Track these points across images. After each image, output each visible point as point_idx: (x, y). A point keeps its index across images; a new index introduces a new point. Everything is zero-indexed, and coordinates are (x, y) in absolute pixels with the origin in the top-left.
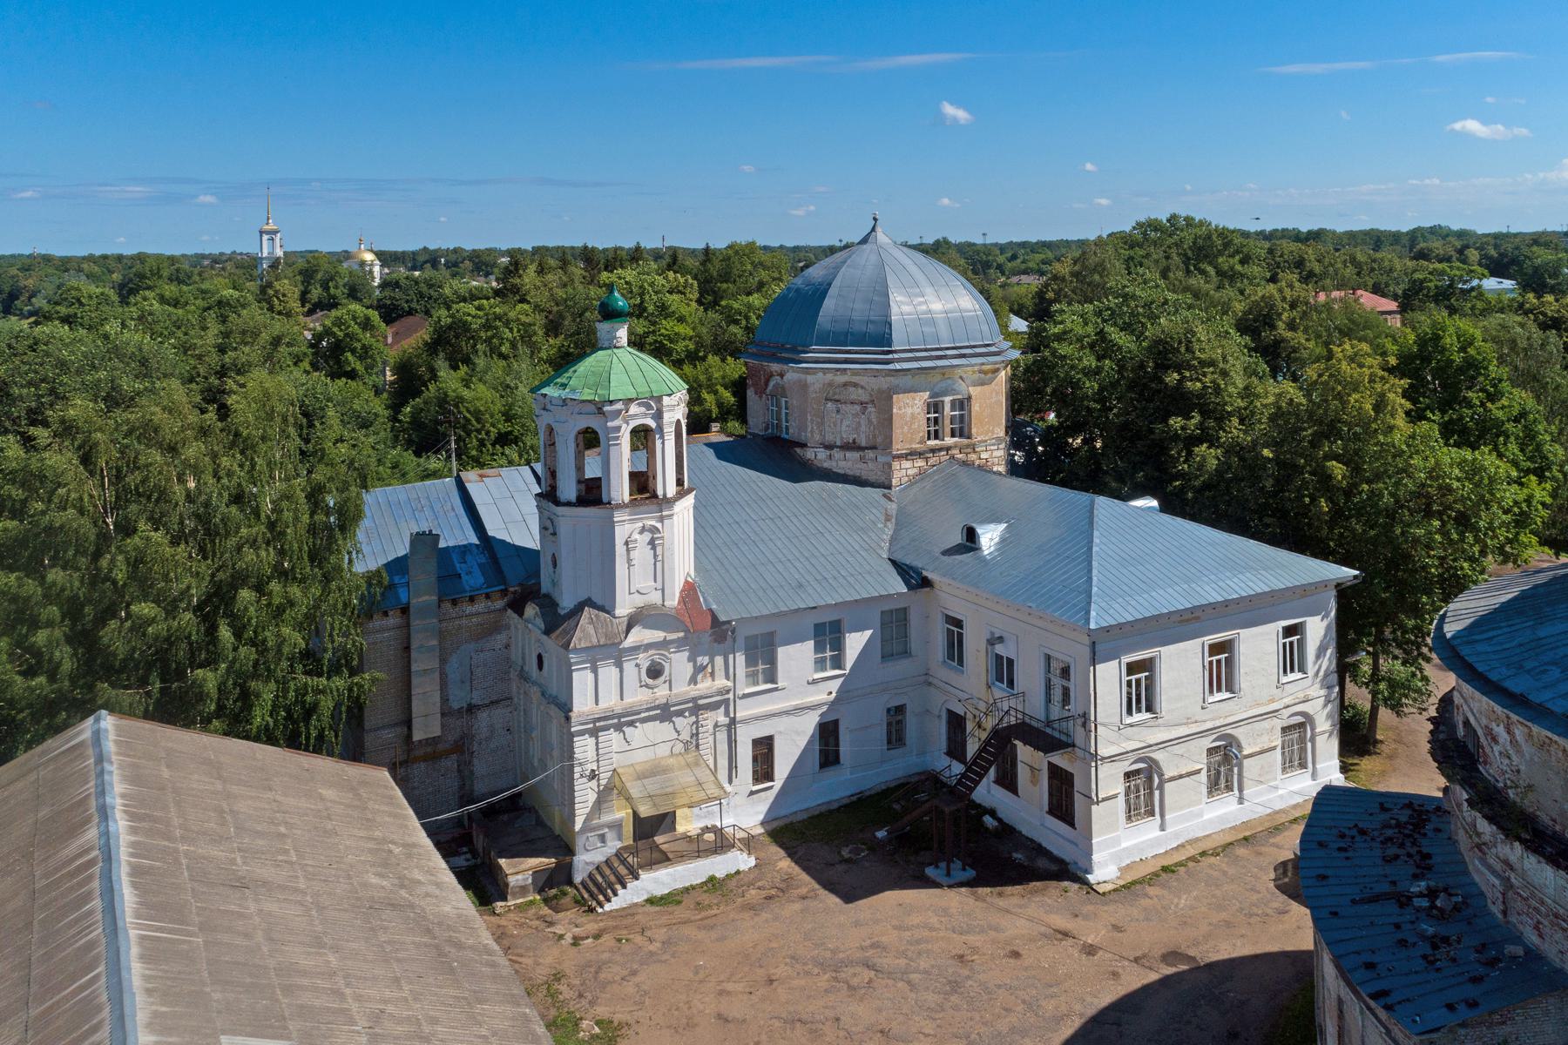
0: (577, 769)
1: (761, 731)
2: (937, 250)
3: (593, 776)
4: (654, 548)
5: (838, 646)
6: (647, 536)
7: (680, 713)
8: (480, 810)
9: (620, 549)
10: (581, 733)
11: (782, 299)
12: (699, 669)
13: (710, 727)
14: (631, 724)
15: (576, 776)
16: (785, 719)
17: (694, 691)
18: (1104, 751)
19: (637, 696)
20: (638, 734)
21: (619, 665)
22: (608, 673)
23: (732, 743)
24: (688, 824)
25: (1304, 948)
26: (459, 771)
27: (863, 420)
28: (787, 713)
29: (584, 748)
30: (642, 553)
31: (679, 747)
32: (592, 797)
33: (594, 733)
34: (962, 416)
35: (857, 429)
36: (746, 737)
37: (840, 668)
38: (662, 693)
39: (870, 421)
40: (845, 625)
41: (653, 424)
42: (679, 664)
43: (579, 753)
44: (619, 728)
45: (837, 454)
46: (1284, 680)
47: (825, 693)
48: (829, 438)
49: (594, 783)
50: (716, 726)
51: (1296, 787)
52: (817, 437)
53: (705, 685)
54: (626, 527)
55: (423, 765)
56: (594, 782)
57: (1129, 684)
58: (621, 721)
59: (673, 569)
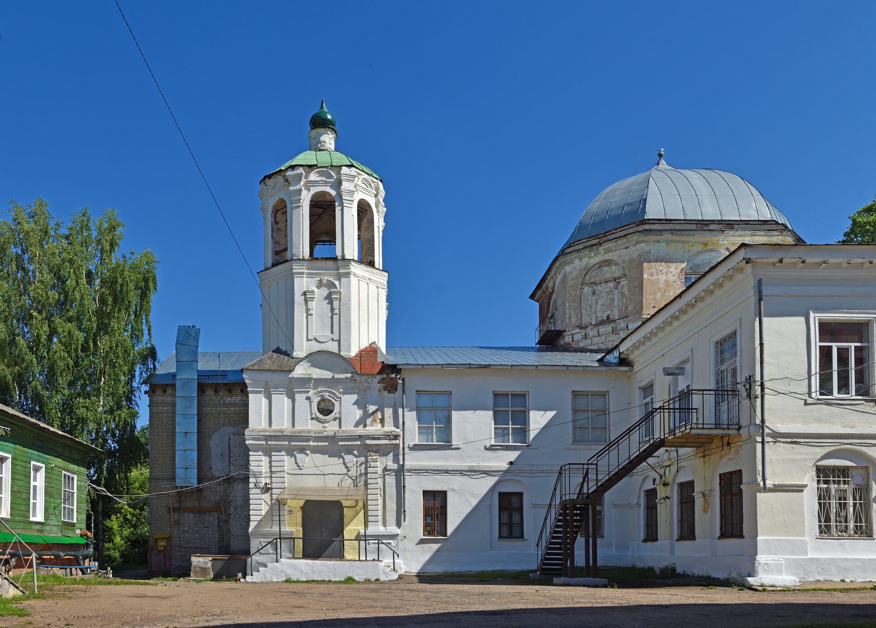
0: (251, 480)
1: (435, 484)
2: (459, 449)
3: (267, 489)
4: (331, 303)
5: (522, 419)
6: (325, 291)
7: (349, 451)
8: (7, 405)
9: (298, 299)
10: (257, 449)
11: (653, 444)
12: (366, 415)
13: (380, 471)
14: (302, 450)
15: (251, 485)
16: (459, 478)
17: (360, 430)
18: (774, 423)
19: (307, 424)
20: (307, 460)
21: (292, 396)
22: (282, 402)
23: (400, 489)
24: (568, 339)
25: (171, 371)
26: (219, 527)
27: (616, 295)
28: (461, 472)
29: (258, 463)
30: (318, 305)
31: (348, 482)
32: (265, 509)
33: (268, 452)
34: (723, 361)
35: (610, 306)
36: (415, 489)
37: (399, 436)
38: (332, 428)
39: (622, 294)
40: (531, 400)
41: (333, 193)
42: (348, 407)
43: (253, 467)
44: (290, 452)
45: (592, 332)
46: (653, 377)
47: (501, 461)
48: (585, 320)
49: (266, 497)
50: (385, 469)
51: (201, 559)
52: (574, 320)
53: (374, 428)
54: (304, 283)
55: (192, 515)
56: (268, 495)
57: (825, 353)
58: (293, 444)
59: (349, 323)
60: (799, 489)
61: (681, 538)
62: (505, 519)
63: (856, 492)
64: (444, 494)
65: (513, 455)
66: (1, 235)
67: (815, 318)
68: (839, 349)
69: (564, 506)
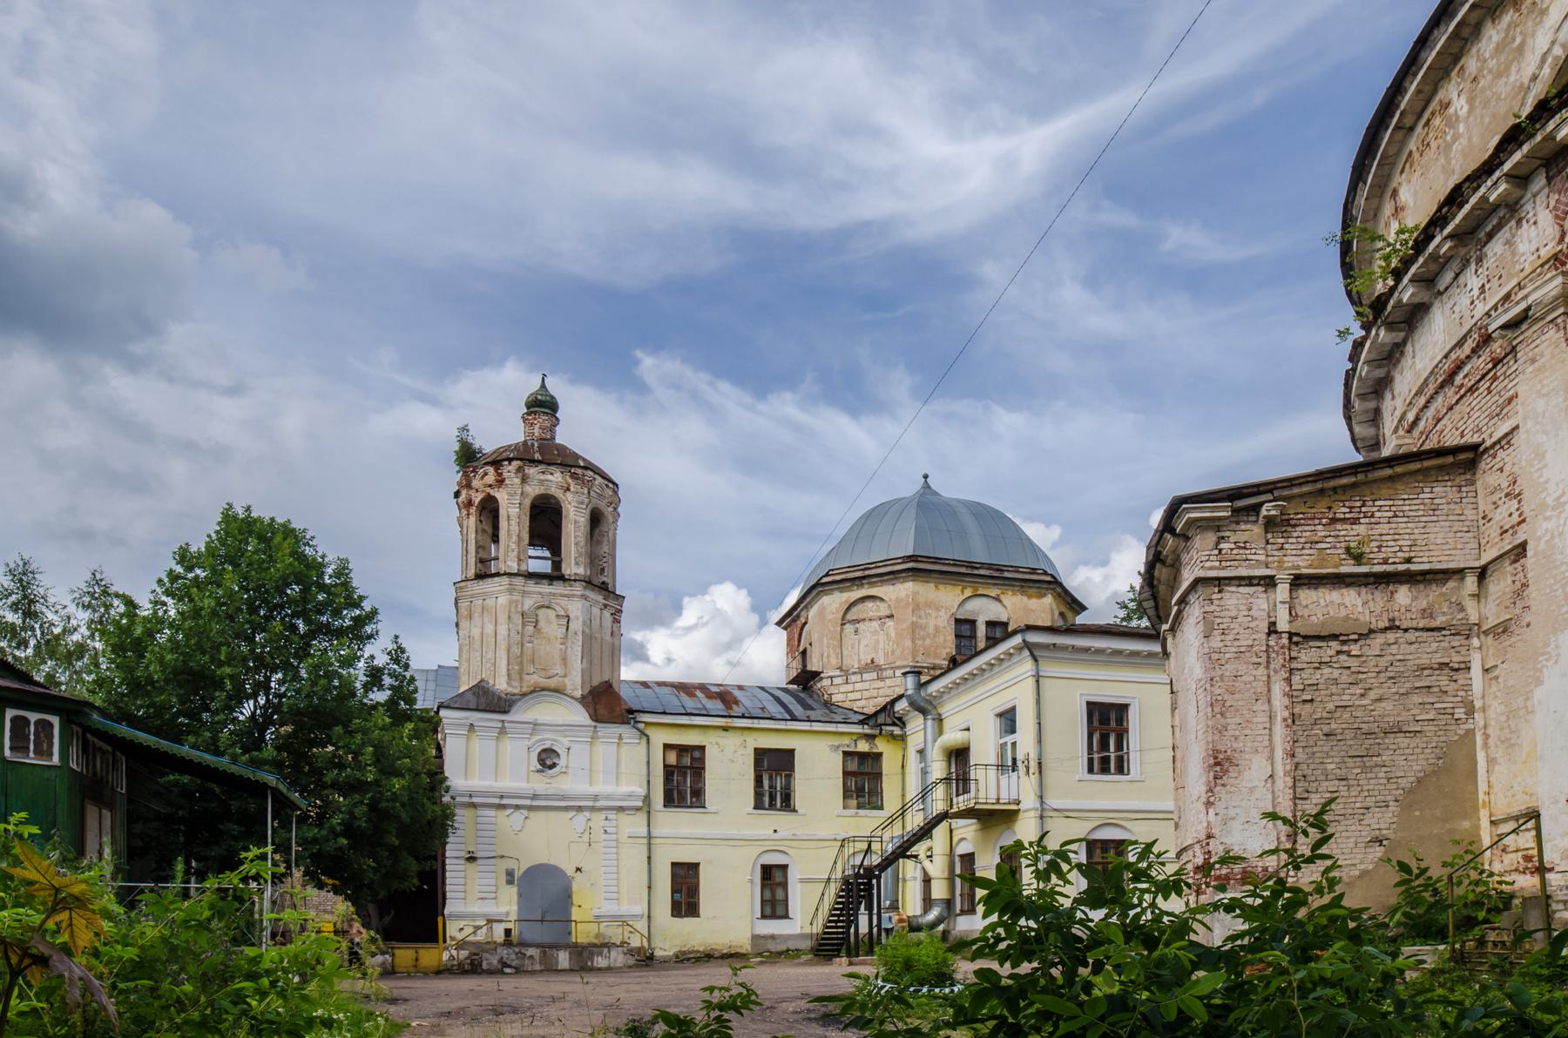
35: (875, 648)
60: (802, 881)
61: (673, 798)
62: (768, 895)
63: (1, 650)
64: (702, 748)
65: (1560, 280)
66: (25, 956)
67: (660, 738)
68: (14, 720)
69: (846, 881)
